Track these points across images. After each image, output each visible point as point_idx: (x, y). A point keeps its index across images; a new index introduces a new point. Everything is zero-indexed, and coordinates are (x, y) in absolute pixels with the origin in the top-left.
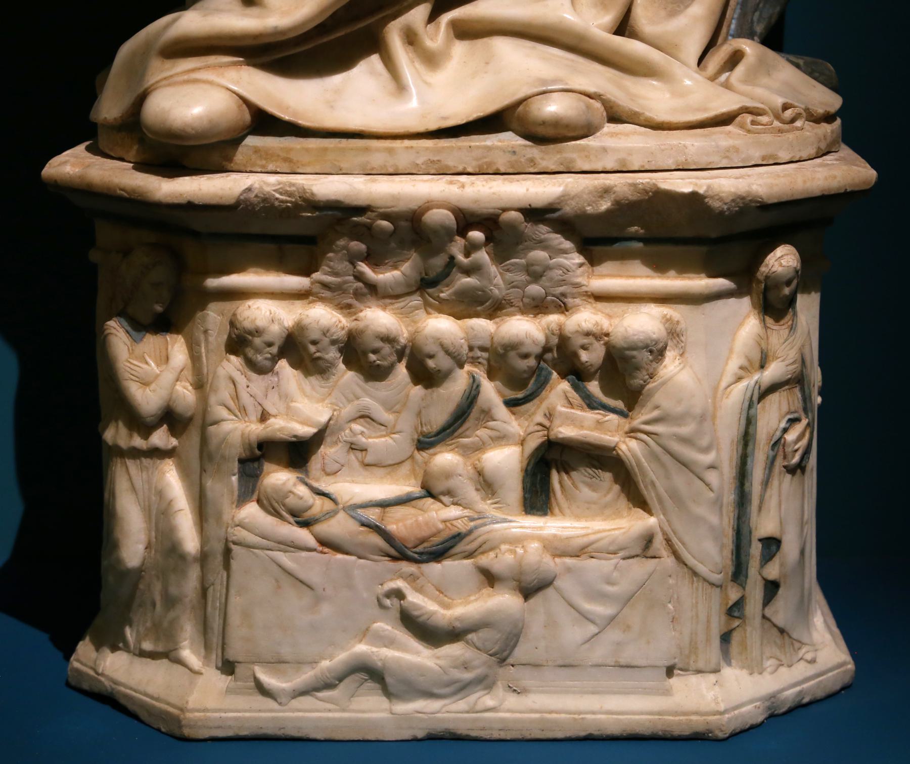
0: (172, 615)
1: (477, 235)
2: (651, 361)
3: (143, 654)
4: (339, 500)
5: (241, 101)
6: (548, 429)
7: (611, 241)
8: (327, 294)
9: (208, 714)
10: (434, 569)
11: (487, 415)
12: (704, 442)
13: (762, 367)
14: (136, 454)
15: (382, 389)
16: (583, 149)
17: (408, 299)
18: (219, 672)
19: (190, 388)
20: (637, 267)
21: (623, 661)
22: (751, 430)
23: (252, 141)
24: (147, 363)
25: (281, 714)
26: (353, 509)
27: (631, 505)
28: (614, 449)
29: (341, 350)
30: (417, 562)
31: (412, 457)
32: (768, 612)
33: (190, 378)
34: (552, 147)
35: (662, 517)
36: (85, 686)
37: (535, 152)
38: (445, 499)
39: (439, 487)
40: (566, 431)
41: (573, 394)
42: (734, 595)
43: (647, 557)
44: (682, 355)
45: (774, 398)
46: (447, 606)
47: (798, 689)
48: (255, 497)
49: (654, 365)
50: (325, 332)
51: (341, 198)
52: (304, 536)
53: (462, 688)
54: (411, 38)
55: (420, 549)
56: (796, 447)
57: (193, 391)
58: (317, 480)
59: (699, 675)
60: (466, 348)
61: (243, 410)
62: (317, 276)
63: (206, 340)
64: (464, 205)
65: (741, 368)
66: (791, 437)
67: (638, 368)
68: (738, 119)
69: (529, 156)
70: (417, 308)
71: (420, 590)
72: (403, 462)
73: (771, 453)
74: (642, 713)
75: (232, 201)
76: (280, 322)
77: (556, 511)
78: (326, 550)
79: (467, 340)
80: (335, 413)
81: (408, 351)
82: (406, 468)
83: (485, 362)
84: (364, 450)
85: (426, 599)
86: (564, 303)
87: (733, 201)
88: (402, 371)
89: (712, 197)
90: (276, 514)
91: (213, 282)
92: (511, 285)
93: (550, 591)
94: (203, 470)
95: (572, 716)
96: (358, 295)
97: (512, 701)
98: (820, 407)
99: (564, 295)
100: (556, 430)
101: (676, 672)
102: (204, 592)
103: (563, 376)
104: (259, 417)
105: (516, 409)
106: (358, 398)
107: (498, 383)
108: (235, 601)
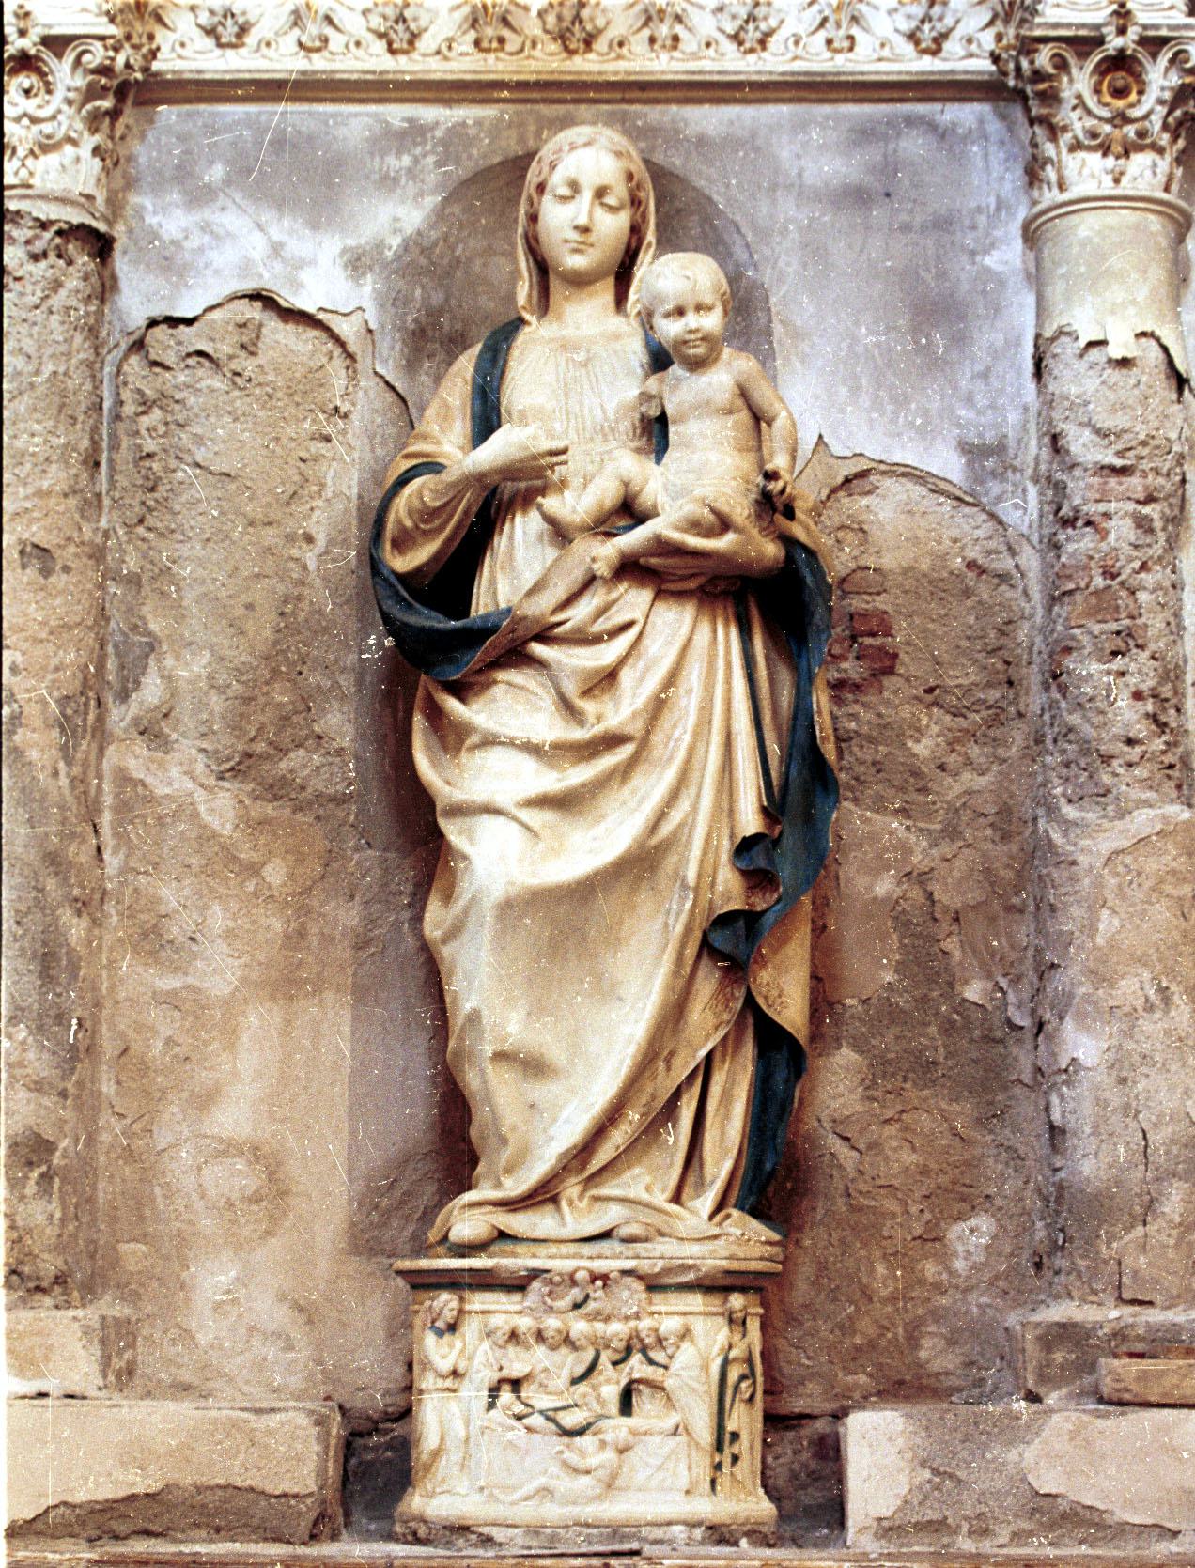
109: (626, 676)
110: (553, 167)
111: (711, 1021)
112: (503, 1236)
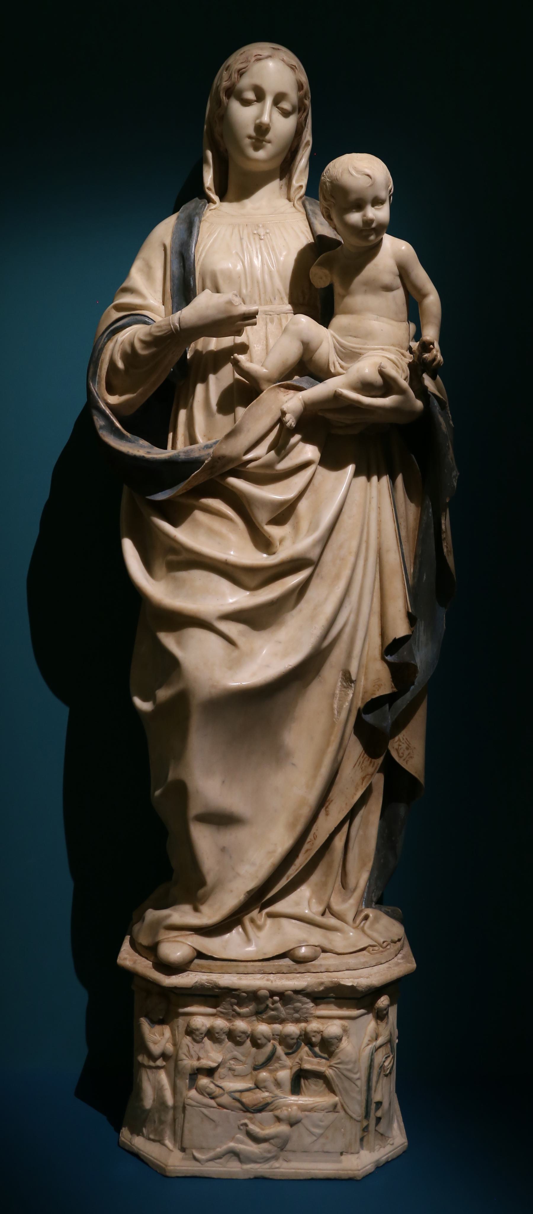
0: (162, 1127)
1: (276, 998)
2: (337, 1042)
3: (149, 1139)
4: (225, 1089)
5: (194, 949)
6: (300, 1064)
7: (323, 998)
8: (222, 1015)
9: (176, 1168)
10: (259, 1115)
11: (279, 1059)
12: (356, 1070)
13: (376, 1039)
14: (150, 1067)
15: (241, 1049)
16: (313, 965)
17: (251, 1018)
18: (179, 1151)
19: (171, 1045)
20: (333, 1006)
21: (325, 1150)
22: (372, 1064)
23: (197, 961)
24: (156, 1036)
25: (202, 1168)
26: (230, 1093)
27: (329, 1092)
28: (324, 1073)
29: (226, 1035)
30: (252, 1113)
31: (251, 1073)
32: (377, 1128)
33: (171, 1041)
34: (303, 965)
35: (340, 1097)
36: (127, 1148)
37: (297, 966)
38: (263, 1090)
39: (261, 1085)
40: (307, 1066)
41: (310, 1052)
42: (365, 1123)
43: (335, 1112)
44: (348, 1038)
45: (381, 1049)
46: (263, 1129)
47: (387, 1156)
48: (195, 1087)
49: (338, 1043)
50: (221, 1030)
51: (228, 986)
52: (212, 1102)
53: (267, 1160)
54: (252, 921)
55: (253, 1108)
56: (388, 1067)
57: (172, 1047)
58: (217, 1081)
59: (352, 1155)
60: (272, 1035)
61: (192, 1056)
62: (219, 1009)
63: (178, 1029)
64: (272, 989)
65: (369, 1041)
66: (386, 1064)
67: (333, 1045)
68: (367, 949)
69: (295, 968)
70: (254, 1020)
71: (253, 1123)
72: (248, 1075)
73: (379, 1071)
74: (332, 1170)
75: (191, 986)
76: (206, 1026)
77: (303, 1093)
78: (220, 1108)
79: (272, 1032)
80: (224, 1057)
81: (250, 1035)
82: (249, 1077)
83: (278, 1040)
84: (234, 1070)
85: (256, 1127)
86: (307, 1020)
87: (366, 987)
88: (248, 1042)
89: (359, 987)
90: (202, 1094)
91: (182, 1010)
92: (288, 1014)
93: (300, 1124)
94: (175, 1076)
95: (306, 1171)
96: (233, 1016)
97: (285, 1164)
98: (398, 1044)
99: (307, 1017)
100: (303, 1065)
101: (344, 1153)
102: (174, 1120)
103: (306, 1044)
104: (197, 1058)
105: (288, 1056)
106: (232, 1052)
107: (283, 1047)
108: (187, 1125)
109: (303, 506)
110: (241, 73)
111: (359, 775)
112: (200, 955)
